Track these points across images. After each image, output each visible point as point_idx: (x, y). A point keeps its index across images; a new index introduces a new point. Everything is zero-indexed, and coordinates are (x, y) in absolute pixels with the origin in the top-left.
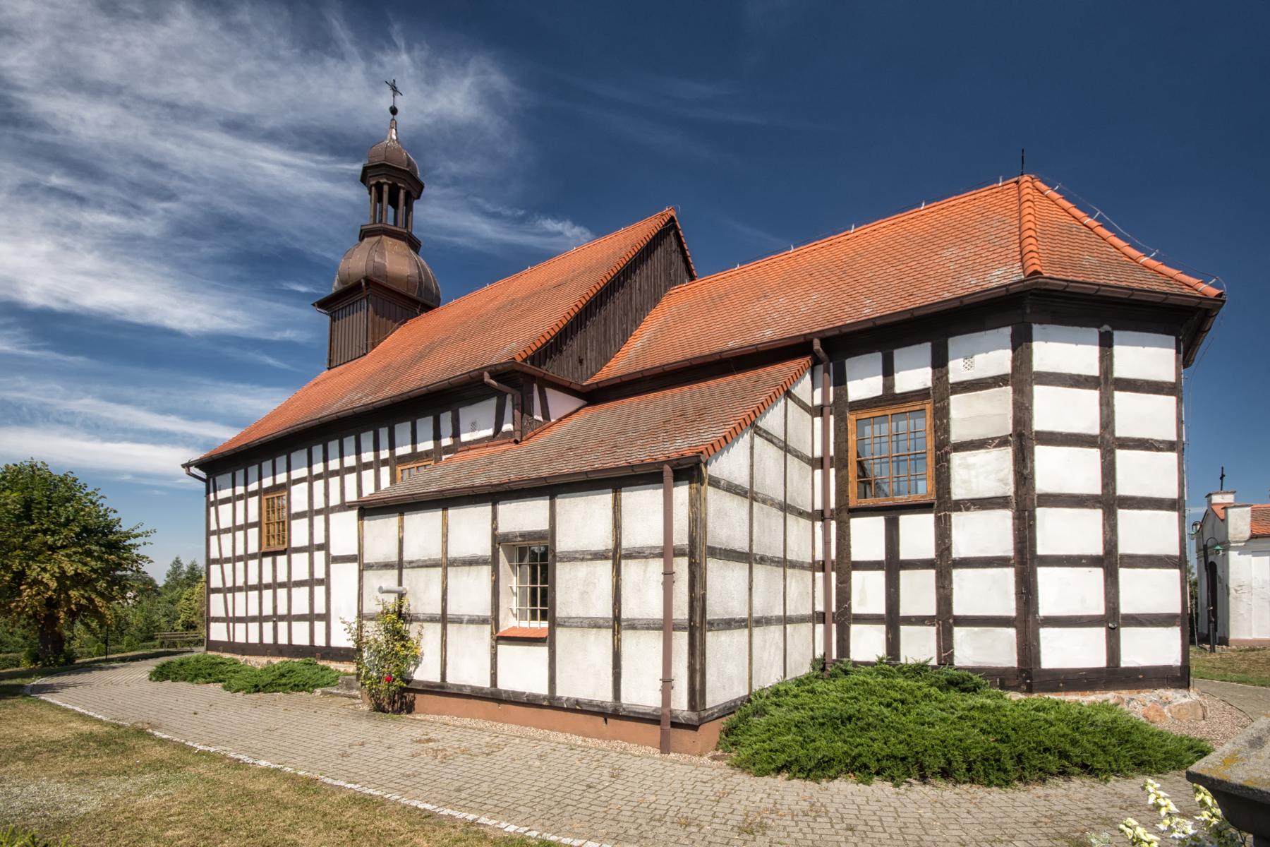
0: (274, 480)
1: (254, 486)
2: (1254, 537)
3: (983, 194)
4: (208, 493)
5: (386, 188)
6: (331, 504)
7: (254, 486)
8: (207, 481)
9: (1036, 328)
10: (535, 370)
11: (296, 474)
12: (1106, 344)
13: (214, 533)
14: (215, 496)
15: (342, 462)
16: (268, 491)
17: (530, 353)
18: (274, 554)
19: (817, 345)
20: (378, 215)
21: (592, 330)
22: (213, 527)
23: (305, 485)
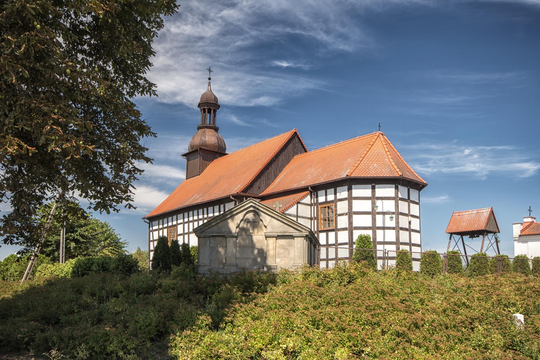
0: (172, 223)
1: (165, 225)
2: (520, 236)
3: (369, 136)
4: (150, 227)
5: (207, 110)
6: (190, 231)
7: (165, 225)
8: (149, 223)
9: (353, 186)
10: (244, 194)
11: (179, 222)
12: (373, 188)
13: (152, 241)
14: (152, 229)
15: (193, 218)
16: (170, 227)
17: (242, 190)
18: (327, 231)
19: (310, 188)
20: (204, 120)
21: (263, 178)
22: (151, 239)
23: (182, 225)
